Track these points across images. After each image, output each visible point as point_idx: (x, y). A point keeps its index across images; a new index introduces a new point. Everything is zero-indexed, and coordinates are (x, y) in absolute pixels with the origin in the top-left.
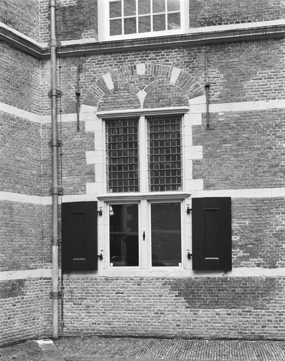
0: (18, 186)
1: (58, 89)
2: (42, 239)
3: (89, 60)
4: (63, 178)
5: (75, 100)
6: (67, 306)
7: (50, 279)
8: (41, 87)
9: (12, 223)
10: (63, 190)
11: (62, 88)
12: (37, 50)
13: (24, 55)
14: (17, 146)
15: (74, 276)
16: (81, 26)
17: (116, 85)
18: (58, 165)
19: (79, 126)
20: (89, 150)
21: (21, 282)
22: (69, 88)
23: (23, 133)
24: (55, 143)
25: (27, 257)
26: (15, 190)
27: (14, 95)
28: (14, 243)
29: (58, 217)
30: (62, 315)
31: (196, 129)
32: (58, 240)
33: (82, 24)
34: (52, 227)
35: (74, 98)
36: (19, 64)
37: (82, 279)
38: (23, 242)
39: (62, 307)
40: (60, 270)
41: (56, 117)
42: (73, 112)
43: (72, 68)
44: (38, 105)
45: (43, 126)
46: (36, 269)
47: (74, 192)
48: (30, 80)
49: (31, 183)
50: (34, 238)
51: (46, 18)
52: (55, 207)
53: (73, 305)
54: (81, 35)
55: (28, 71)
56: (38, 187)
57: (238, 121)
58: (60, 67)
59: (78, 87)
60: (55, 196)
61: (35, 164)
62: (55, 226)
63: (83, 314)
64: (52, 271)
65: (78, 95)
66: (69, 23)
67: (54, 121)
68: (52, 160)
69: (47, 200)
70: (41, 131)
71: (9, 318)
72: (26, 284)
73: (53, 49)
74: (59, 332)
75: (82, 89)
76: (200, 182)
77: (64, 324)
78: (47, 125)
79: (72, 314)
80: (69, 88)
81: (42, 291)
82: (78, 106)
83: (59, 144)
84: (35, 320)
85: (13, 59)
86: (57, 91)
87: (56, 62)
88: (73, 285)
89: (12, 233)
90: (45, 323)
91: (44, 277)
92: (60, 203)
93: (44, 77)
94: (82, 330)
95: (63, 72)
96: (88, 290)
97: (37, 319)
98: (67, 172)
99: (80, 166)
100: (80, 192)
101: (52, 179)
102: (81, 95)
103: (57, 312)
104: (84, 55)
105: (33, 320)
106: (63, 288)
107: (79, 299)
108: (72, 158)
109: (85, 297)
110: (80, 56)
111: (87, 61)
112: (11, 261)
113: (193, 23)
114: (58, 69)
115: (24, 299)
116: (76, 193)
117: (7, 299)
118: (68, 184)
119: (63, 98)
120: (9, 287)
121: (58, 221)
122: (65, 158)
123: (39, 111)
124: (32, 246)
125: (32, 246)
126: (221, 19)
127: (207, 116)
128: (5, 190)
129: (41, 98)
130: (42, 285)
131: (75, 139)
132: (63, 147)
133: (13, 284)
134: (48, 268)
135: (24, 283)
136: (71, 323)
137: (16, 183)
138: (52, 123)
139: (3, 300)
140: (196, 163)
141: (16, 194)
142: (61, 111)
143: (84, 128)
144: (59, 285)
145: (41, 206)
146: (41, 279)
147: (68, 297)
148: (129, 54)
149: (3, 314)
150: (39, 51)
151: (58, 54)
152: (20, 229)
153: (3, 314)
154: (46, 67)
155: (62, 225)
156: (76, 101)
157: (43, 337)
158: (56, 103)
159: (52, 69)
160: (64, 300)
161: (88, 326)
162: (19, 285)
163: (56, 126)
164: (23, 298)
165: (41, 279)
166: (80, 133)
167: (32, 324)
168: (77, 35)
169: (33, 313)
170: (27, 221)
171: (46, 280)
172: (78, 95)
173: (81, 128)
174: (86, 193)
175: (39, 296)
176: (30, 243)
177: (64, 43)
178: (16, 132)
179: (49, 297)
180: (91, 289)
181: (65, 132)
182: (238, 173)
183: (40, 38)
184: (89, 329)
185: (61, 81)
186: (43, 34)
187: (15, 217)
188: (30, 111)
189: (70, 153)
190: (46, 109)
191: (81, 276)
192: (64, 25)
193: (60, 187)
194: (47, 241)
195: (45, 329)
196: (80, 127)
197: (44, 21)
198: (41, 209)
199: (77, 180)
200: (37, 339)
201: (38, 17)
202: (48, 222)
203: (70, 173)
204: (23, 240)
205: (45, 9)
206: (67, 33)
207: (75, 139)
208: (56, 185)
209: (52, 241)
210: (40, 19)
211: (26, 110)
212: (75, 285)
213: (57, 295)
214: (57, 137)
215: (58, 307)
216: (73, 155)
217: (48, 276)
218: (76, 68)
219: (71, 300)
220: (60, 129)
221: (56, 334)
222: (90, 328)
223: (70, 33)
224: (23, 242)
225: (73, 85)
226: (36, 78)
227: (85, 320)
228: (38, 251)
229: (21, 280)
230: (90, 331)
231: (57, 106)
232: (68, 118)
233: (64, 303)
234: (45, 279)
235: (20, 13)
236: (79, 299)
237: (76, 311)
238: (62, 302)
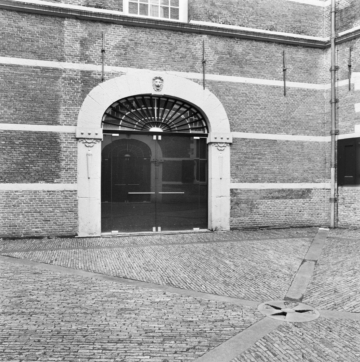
0: (308, 131)
1: (336, 65)
2: (325, 164)
3: (358, 41)
4: (339, 123)
5: (347, 70)
6: (340, 207)
7: (330, 189)
8: (325, 66)
9: (303, 154)
10: (338, 131)
11: (338, 64)
12: (322, 44)
13: (313, 49)
14: (307, 107)
15: (346, 188)
16: (353, 19)
18: (335, 115)
20: (357, 103)
21: (309, 190)
22: (344, 63)
23: (311, 98)
24: (333, 101)
25: (313, 175)
26: (305, 134)
27: (304, 76)
28: (304, 166)
29: (335, 149)
30: (337, 213)
32: (335, 165)
33: (354, 17)
34: (331, 156)
35: (347, 69)
36: (309, 56)
37: (351, 191)
38: (310, 165)
39: (337, 208)
40: (336, 184)
41: (335, 84)
42: (346, 79)
43: (346, 49)
44: (323, 78)
45: (326, 91)
46: (320, 182)
47: (347, 132)
48: (317, 64)
49: (317, 129)
50: (319, 163)
51: (329, 20)
52: (333, 143)
53: (344, 207)
54: (352, 26)
55: (315, 58)
56: (322, 130)
58: (338, 51)
59: (350, 61)
60: (334, 136)
61: (320, 116)
62: (333, 155)
63: (351, 214)
64: (331, 184)
65: (350, 66)
66: (344, 20)
67: (333, 87)
68: (332, 113)
69: (328, 139)
70: (325, 94)
71: (300, 212)
72: (312, 192)
73: (333, 40)
74: (335, 224)
75: (352, 62)
77: (338, 219)
78: (329, 90)
79: (344, 213)
80: (344, 63)
81: (324, 197)
82: (350, 73)
83: (336, 101)
84: (319, 215)
85: (304, 54)
86: (335, 67)
87: (335, 48)
88: (345, 194)
89: (303, 160)
90: (326, 218)
91: (326, 188)
92: (336, 140)
93: (325, 59)
94: (350, 224)
95: (339, 54)
96: (355, 198)
97: (320, 215)
98: (341, 119)
99: (351, 114)
100: (350, 132)
101: (331, 125)
102: (352, 66)
103: (333, 211)
104: (355, 39)
105: (317, 214)
106: (338, 196)
107: (349, 203)
108: (345, 109)
109: (353, 202)
110: (351, 40)
111: (356, 42)
112: (302, 177)
114: (336, 52)
115: (311, 201)
116: (348, 132)
117: (299, 200)
118: (342, 127)
119: (339, 71)
120: (300, 193)
121: (335, 152)
122: (341, 110)
123: (323, 82)
124: (317, 168)
125: (317, 168)
128: (298, 134)
129: (325, 73)
130: (325, 193)
131: (347, 97)
132: (339, 103)
133: (303, 191)
134: (328, 182)
135: (311, 191)
136: (343, 219)
137: (306, 130)
138: (332, 89)
139: (296, 200)
141: (306, 136)
142: (338, 79)
143: (354, 88)
144: (335, 194)
145: (324, 143)
146: (324, 189)
147: (341, 202)
148: (16, 236)
149: (296, 208)
150: (323, 44)
151: (336, 42)
152: (309, 158)
153: (296, 208)
154: (328, 52)
155: (338, 154)
156: (348, 71)
157: (324, 226)
158: (335, 75)
159: (332, 53)
160: (339, 204)
161: (355, 222)
162: (307, 192)
163: (335, 90)
164: (310, 200)
165: (324, 189)
166: (350, 92)
167: (316, 217)
168: (349, 26)
169: (318, 210)
170: (314, 152)
171: (327, 190)
172: (350, 66)
173: (351, 88)
174: (354, 132)
175: (322, 200)
176: (315, 166)
177: (340, 34)
178: (306, 98)
179: (329, 201)
180: (357, 197)
181: (341, 92)
183: (325, 35)
184: (355, 224)
185: (338, 60)
186: (326, 32)
187: (305, 150)
188: (316, 83)
189: (344, 106)
190: (328, 79)
191: (351, 188)
192: (341, 22)
193: (337, 129)
194: (328, 165)
195: (326, 221)
196: (351, 88)
197: (327, 23)
198: (325, 145)
199: (349, 124)
200: (320, 227)
201: (323, 22)
202: (329, 153)
203: (344, 120)
204: (311, 165)
205: (328, 15)
206: (342, 27)
207: (347, 97)
208: (334, 129)
209: (331, 165)
210: (325, 22)
211: (313, 83)
212: (346, 194)
213: (334, 200)
214: (335, 97)
215: (334, 208)
216: (346, 108)
217: (329, 188)
218: (349, 48)
219: (343, 204)
220: (337, 92)
221: (332, 225)
222: (356, 224)
223: (345, 26)
224: (310, 165)
225: (346, 60)
226: (321, 61)
227: (353, 218)
228: (321, 172)
229: (309, 189)
230: (356, 226)
231: (335, 76)
232: (342, 83)
233: (339, 205)
234: (326, 189)
235: (310, 23)
236: (349, 203)
237: (346, 212)
238: (337, 205)
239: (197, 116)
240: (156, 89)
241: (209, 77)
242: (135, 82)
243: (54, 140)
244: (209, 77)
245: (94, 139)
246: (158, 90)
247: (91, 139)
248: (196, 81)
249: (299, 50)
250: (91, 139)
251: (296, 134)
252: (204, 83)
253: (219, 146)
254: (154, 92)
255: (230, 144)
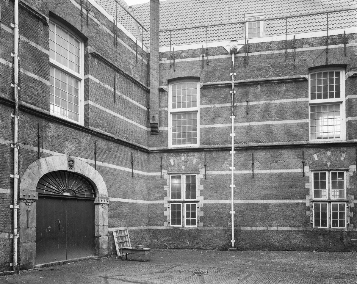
7: (152, 134)
17: (174, 163)
19: (161, 177)
31: (201, 180)
57: (215, 178)
64: (200, 78)
76: (202, 198)
113: (201, 143)
126: (210, 143)
127: (205, 175)
140: (201, 191)
182: (215, 195)
239: (90, 185)
240: (70, 168)
241: (98, 163)
242: (56, 162)
243: (2, 200)
244: (98, 163)
245: (33, 200)
246: (71, 168)
247: (30, 200)
248: (91, 165)
249: (123, 82)
250: (30, 200)
251: (136, 199)
252: (95, 166)
253: (103, 205)
254: (68, 170)
255: (108, 204)
